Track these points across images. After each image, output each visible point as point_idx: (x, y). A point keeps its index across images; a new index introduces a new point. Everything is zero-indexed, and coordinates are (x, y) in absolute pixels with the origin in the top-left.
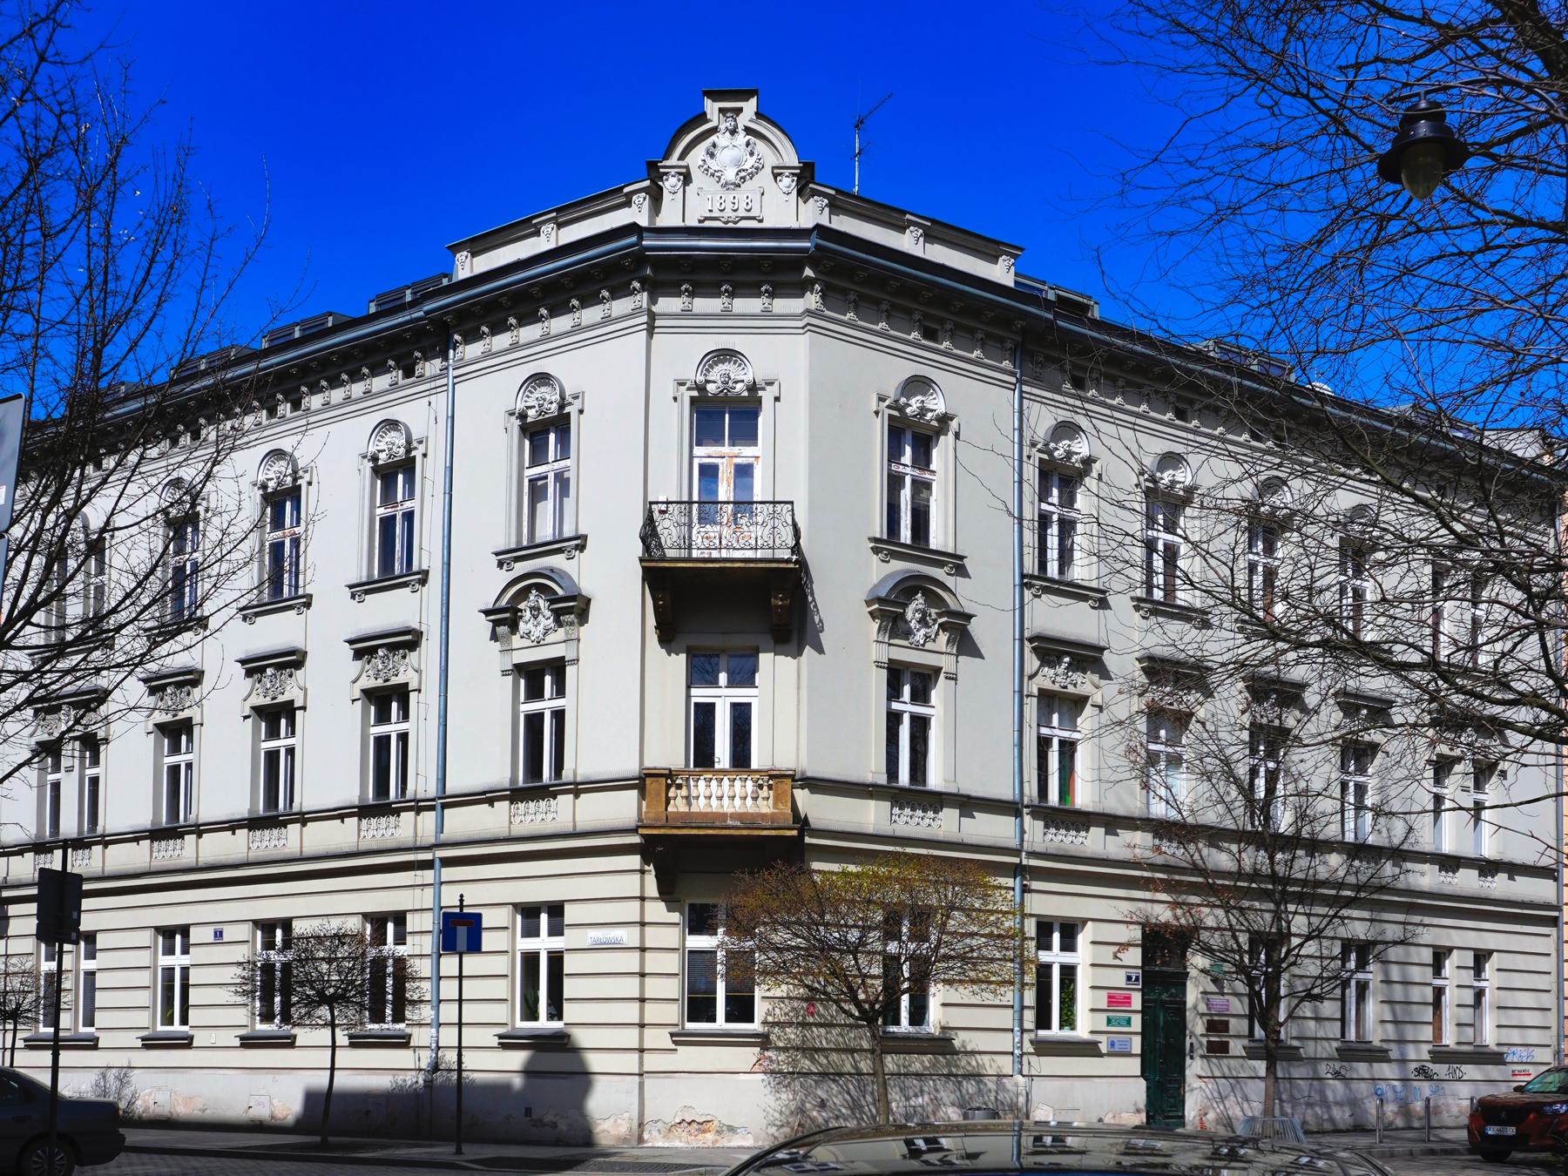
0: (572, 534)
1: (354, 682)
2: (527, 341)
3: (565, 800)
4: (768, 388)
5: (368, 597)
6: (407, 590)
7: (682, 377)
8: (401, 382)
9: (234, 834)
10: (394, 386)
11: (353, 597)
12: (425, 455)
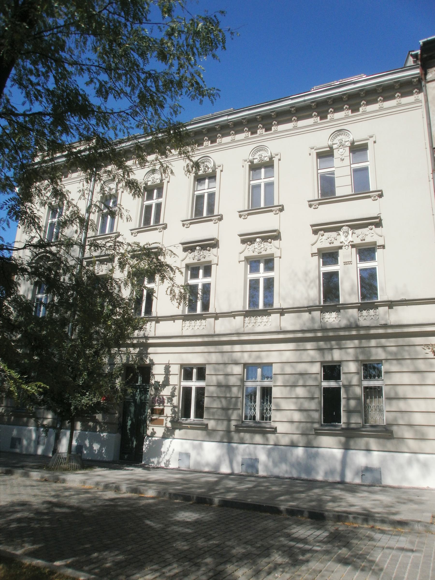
3: (275, 317)
5: (320, 207)
6: (211, 223)
7: (245, 158)
9: (174, 322)
11: (132, 234)
12: (168, 182)
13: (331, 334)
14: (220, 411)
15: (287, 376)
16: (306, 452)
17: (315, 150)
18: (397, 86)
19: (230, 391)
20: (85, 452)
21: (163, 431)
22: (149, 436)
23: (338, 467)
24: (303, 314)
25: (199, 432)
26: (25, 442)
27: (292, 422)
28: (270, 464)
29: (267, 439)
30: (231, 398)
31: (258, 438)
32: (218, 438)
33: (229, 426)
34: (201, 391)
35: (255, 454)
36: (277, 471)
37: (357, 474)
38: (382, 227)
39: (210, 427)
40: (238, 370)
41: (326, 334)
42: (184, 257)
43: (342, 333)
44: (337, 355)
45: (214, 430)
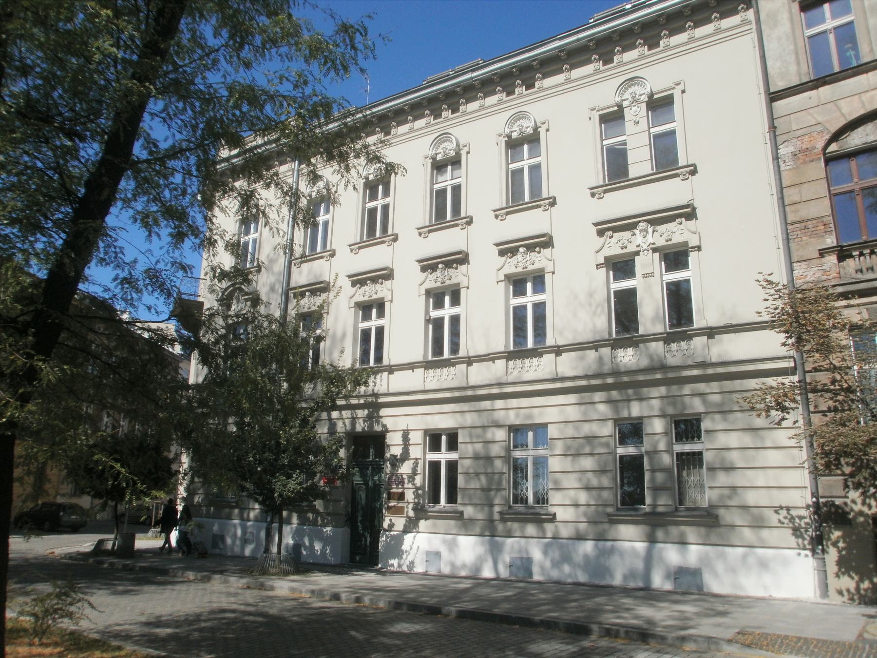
0: (685, 164)
1: (421, 285)
2: (629, 60)
4: (543, 126)
8: (433, 122)
9: (494, 362)
10: (500, 102)
13: (626, 379)
14: (479, 492)
15: (569, 441)
16: (596, 546)
17: (597, 111)
18: (425, 103)
19: (492, 464)
20: (305, 553)
21: (404, 522)
22: (385, 530)
23: (640, 565)
24: (588, 352)
25: (452, 522)
26: (229, 541)
27: (576, 505)
28: (548, 564)
29: (543, 531)
30: (494, 474)
31: (531, 529)
32: (478, 530)
33: (491, 513)
34: (452, 466)
35: (527, 552)
36: (555, 574)
37: (668, 576)
38: (697, 219)
39: (466, 516)
40: (501, 435)
41: (619, 380)
42: (422, 280)
43: (641, 378)
44: (636, 410)
45: (471, 520)
